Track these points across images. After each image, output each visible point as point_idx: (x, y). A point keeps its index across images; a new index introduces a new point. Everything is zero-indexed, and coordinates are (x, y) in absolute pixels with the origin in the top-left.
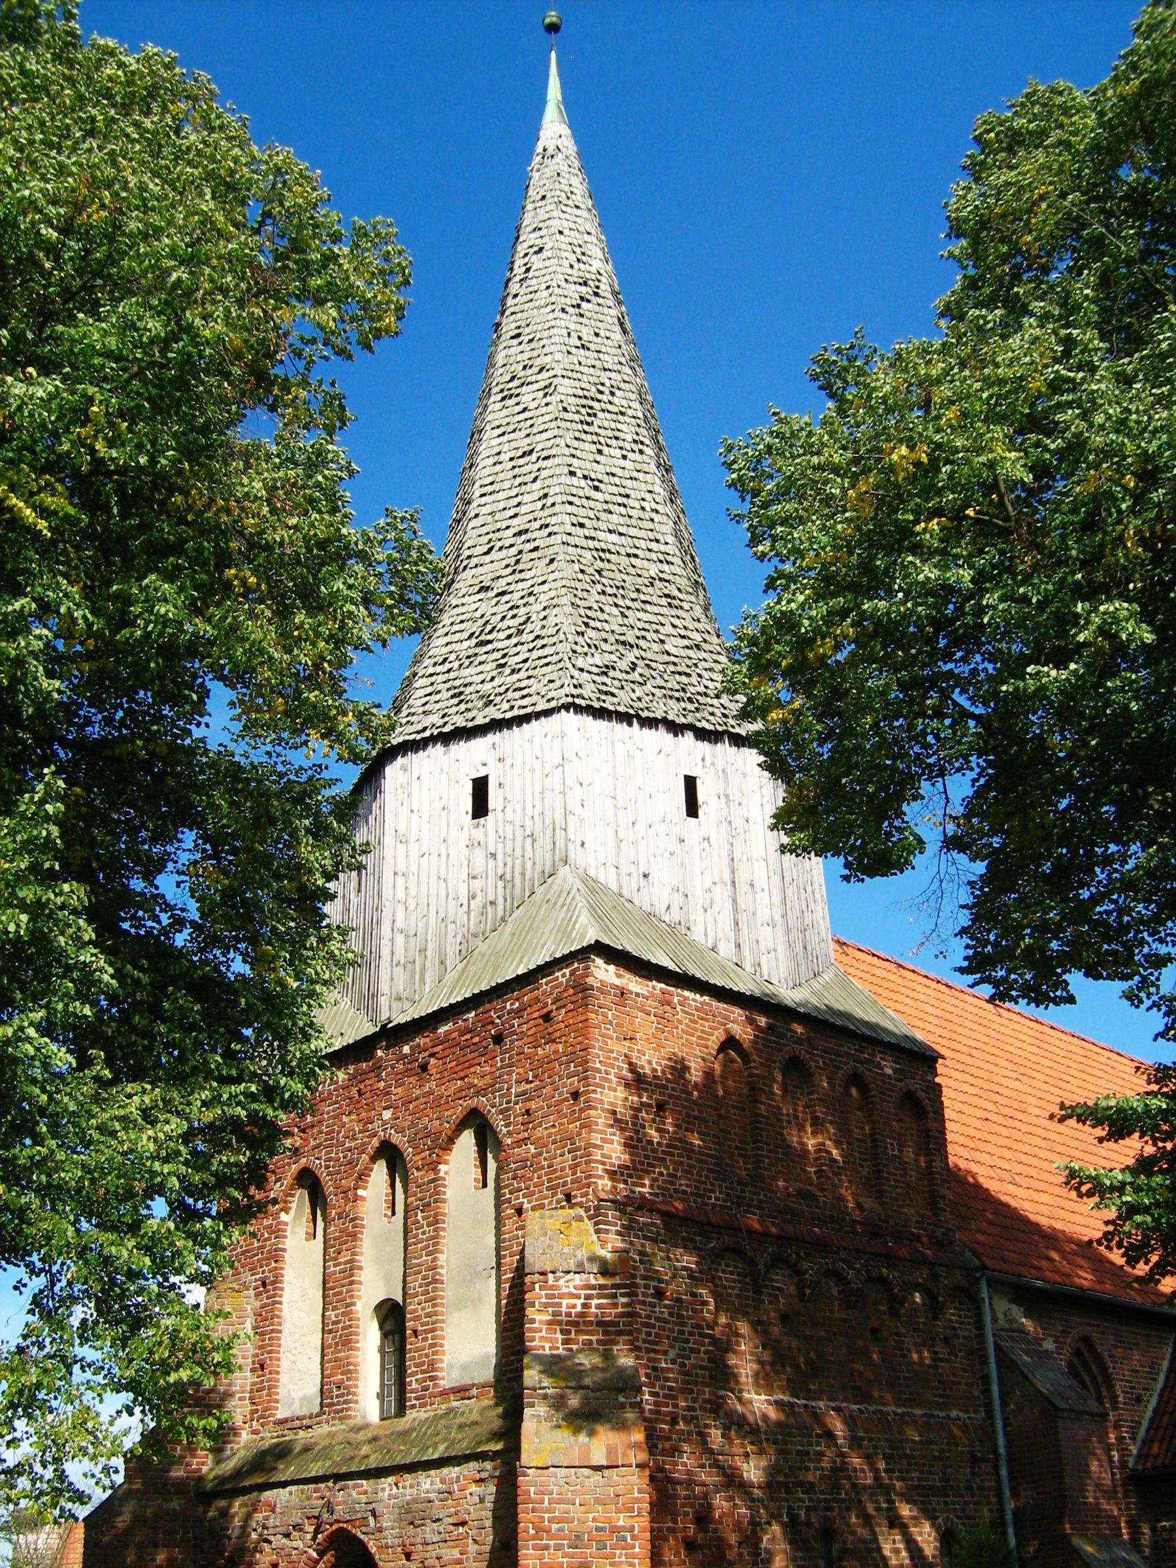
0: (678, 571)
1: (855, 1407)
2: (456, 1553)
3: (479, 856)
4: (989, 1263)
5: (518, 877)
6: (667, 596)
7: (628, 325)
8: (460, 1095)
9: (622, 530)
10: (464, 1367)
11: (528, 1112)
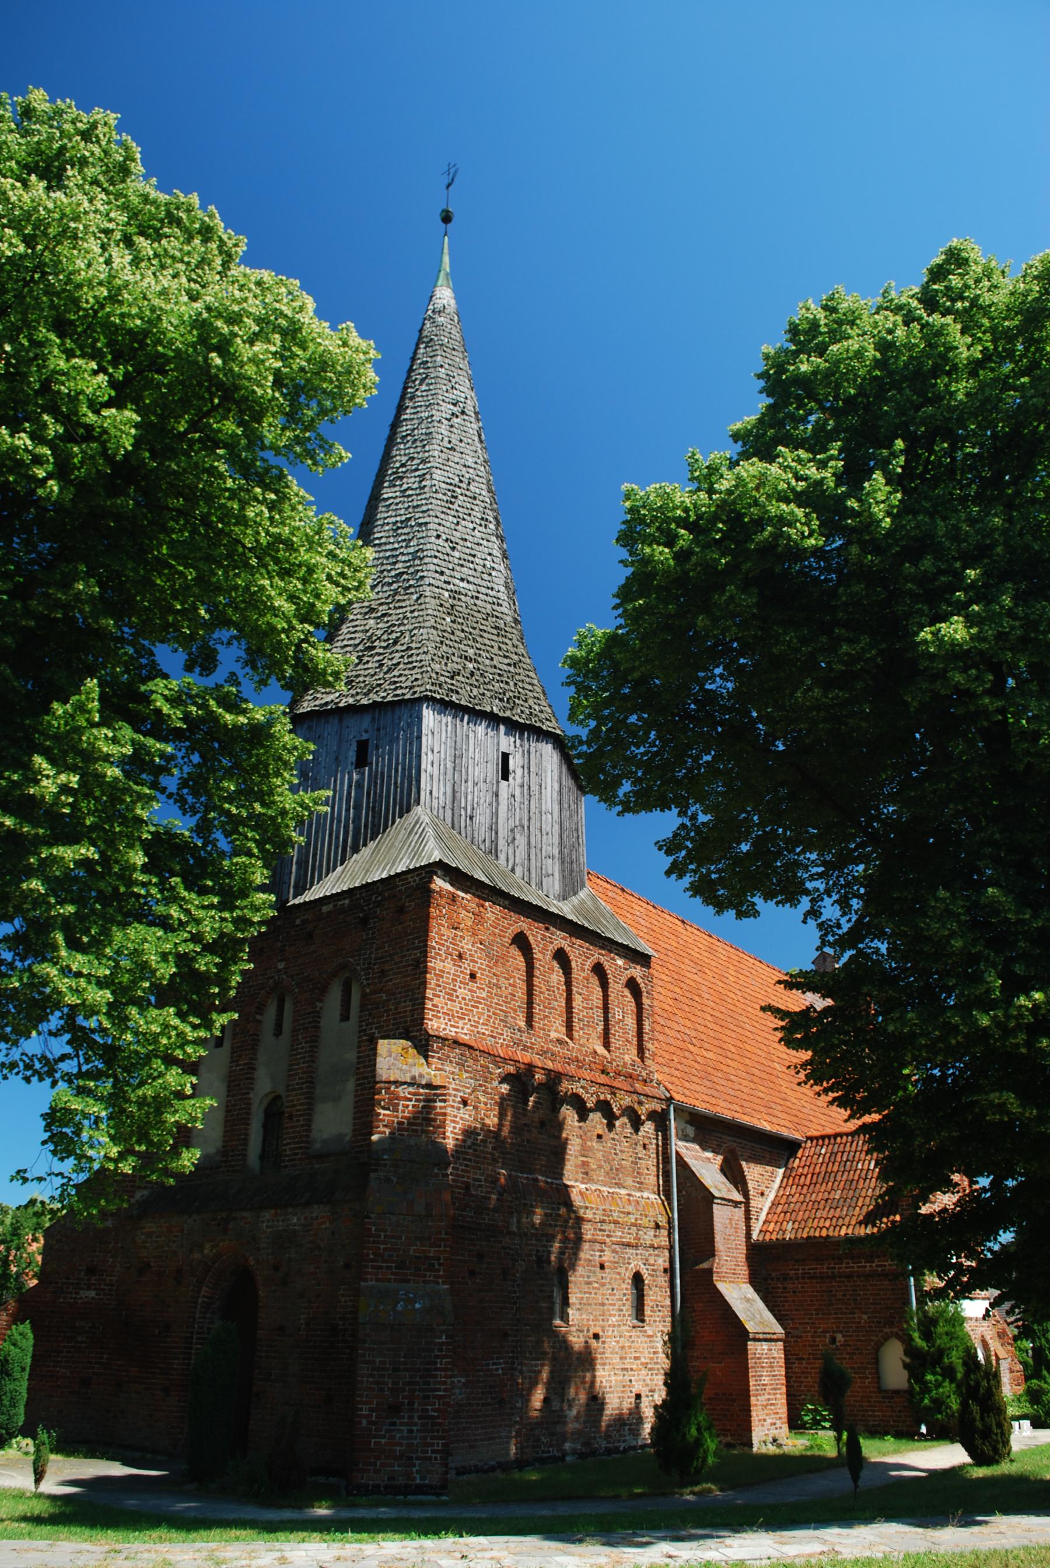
0: (506, 611)
1: (583, 1186)
4: (676, 1096)
6: (496, 628)
7: (483, 437)
9: (471, 579)
11: (382, 972)
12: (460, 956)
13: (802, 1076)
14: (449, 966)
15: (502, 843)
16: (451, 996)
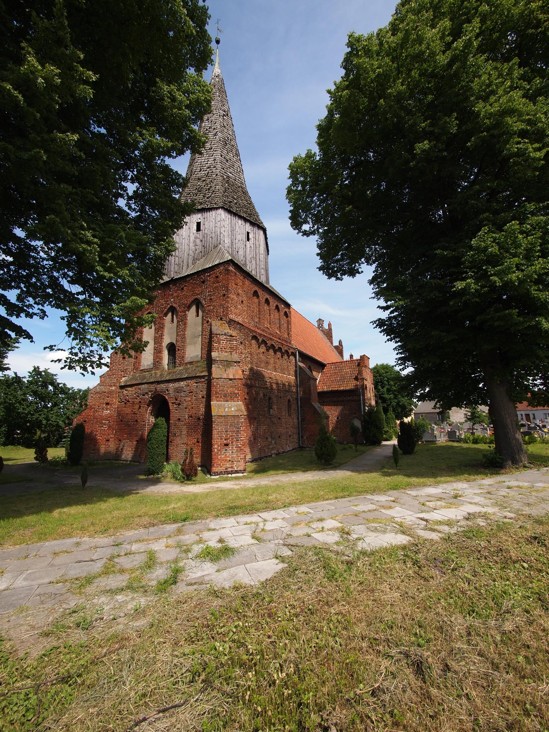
2: (190, 399)
3: (198, 241)
5: (208, 247)
8: (193, 295)
10: (191, 358)
12: (238, 294)
13: (375, 325)
14: (235, 297)
15: (247, 262)
16: (236, 307)
